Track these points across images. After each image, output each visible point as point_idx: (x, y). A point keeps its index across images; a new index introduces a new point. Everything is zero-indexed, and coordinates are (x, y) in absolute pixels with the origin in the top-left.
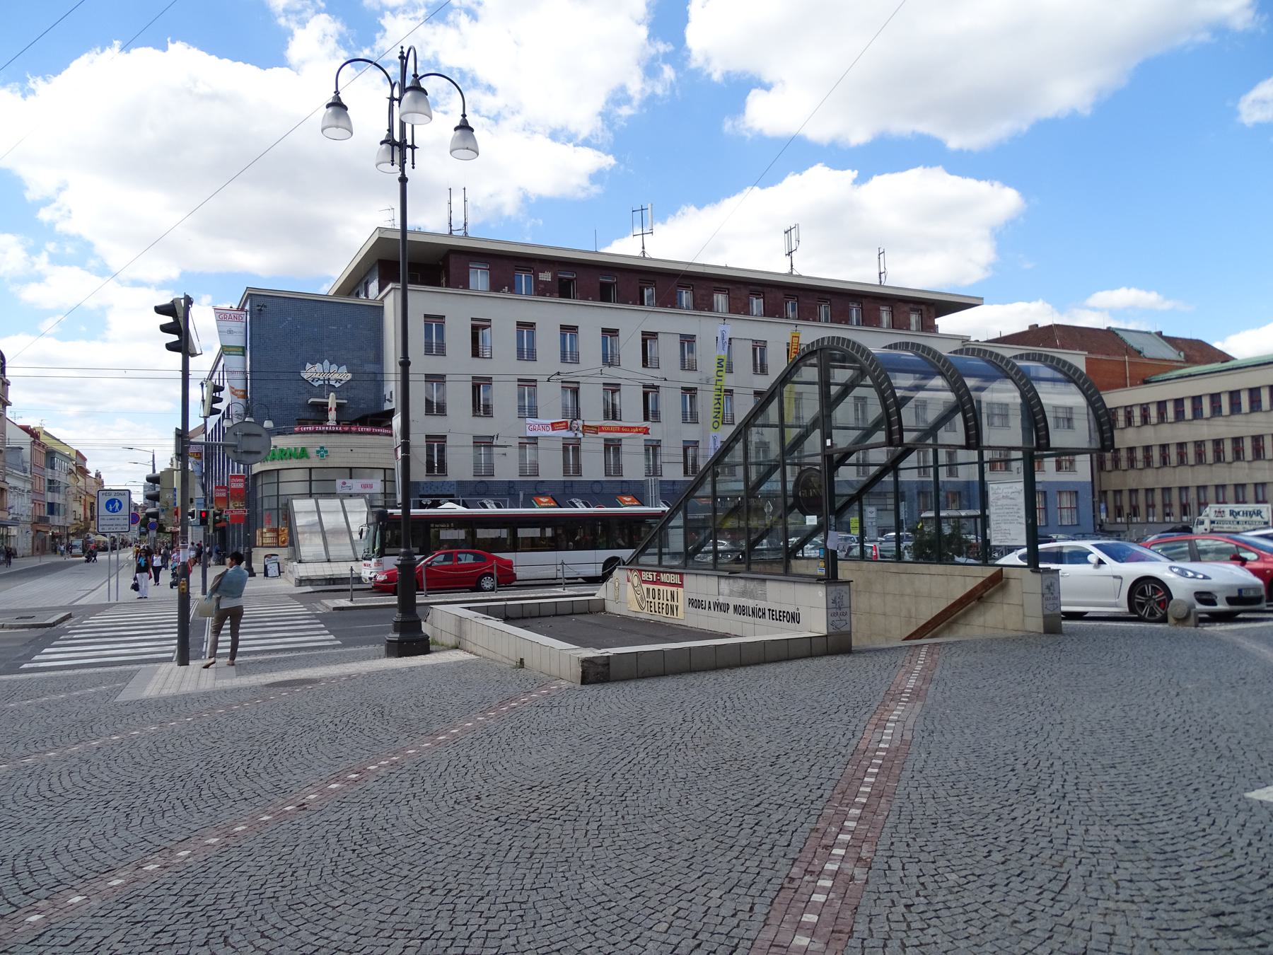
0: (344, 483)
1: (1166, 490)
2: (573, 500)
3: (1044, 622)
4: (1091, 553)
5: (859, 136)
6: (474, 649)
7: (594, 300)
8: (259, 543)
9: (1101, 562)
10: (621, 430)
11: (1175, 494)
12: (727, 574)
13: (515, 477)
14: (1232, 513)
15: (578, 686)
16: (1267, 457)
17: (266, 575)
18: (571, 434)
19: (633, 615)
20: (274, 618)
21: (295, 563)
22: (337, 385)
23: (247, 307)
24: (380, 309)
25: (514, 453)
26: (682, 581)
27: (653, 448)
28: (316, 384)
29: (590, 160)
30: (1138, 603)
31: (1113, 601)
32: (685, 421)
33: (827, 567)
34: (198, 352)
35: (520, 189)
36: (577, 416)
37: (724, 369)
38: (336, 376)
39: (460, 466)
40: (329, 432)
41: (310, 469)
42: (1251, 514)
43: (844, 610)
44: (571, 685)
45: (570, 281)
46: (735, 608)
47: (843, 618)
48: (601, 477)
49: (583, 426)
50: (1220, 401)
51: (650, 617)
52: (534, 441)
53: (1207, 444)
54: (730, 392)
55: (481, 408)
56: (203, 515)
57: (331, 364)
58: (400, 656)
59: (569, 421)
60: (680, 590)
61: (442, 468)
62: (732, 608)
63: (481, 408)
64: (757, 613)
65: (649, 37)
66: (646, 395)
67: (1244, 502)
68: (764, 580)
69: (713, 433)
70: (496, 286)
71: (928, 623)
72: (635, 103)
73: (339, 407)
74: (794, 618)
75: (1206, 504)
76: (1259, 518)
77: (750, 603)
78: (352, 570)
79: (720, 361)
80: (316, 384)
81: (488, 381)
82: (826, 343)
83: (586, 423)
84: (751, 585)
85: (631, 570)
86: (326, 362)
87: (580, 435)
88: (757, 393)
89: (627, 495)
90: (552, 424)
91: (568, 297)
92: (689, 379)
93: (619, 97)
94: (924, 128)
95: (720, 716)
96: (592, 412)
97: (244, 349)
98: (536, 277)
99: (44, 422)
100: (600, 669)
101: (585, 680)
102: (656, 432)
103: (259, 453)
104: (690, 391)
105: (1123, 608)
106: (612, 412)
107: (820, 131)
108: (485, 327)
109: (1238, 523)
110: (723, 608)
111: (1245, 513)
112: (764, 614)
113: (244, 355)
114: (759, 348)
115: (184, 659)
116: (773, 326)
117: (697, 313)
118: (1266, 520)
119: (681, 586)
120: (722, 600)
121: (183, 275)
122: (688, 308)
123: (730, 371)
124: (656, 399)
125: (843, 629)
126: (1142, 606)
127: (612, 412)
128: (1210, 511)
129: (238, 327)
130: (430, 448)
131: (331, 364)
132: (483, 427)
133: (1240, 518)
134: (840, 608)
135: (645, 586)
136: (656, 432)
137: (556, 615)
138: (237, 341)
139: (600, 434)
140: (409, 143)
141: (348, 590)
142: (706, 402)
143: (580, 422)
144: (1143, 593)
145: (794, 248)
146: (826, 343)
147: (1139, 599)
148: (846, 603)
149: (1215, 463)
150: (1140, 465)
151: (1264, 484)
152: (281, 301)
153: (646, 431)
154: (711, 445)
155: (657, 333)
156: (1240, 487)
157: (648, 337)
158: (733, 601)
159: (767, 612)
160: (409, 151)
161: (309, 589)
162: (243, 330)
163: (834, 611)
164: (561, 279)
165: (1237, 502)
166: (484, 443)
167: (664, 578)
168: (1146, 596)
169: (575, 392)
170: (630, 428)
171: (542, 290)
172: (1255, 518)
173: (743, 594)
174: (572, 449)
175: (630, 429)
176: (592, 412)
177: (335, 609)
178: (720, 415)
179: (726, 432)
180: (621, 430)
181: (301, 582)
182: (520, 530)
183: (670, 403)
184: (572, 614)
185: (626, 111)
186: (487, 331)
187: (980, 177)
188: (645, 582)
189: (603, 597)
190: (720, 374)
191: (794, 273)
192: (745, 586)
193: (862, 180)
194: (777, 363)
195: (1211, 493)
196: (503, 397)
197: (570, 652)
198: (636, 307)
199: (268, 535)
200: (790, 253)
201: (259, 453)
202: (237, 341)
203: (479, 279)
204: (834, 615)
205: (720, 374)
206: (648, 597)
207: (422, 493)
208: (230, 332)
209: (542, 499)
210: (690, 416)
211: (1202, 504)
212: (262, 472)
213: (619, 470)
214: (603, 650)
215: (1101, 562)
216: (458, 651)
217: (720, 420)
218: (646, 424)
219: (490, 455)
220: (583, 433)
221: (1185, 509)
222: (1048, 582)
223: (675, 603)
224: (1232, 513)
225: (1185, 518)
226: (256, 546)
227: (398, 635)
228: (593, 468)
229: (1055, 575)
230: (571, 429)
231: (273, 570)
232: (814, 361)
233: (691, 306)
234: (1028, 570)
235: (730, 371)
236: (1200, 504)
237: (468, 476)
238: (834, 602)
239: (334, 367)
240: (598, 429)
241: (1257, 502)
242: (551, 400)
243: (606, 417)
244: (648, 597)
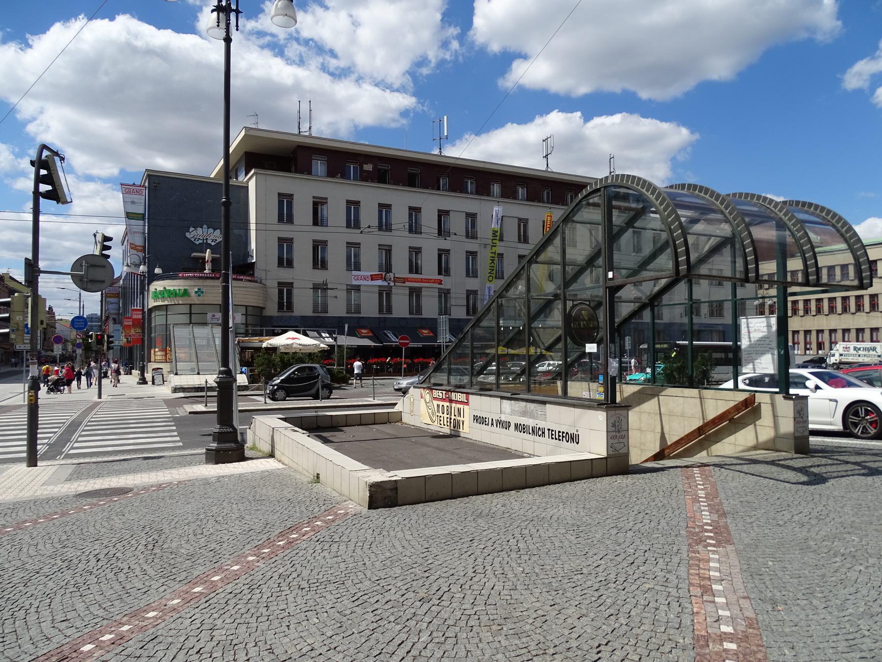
0: (214, 316)
1: (807, 332)
2: (385, 332)
3: (795, 444)
4: (808, 379)
5: (583, 90)
6: (283, 459)
8: (152, 360)
9: (817, 387)
10: (422, 281)
11: (814, 334)
12: (509, 395)
13: (343, 314)
14: (855, 348)
15: (365, 510)
16: (865, 311)
17: (153, 383)
18: (385, 284)
19: (426, 426)
20: (139, 421)
21: (172, 375)
22: (213, 244)
23: (147, 184)
24: (246, 188)
25: (343, 295)
26: (467, 399)
27: (444, 295)
28: (197, 243)
29: (405, 101)
30: (852, 423)
31: (829, 419)
32: (468, 275)
33: (606, 392)
34: (69, 200)
35: (353, 120)
36: (389, 269)
38: (212, 237)
39: (303, 305)
40: (207, 278)
41: (191, 305)
42: (868, 349)
43: (623, 433)
44: (359, 508)
45: (386, 171)
46: (516, 426)
47: (621, 440)
48: (406, 315)
50: (848, 269)
51: (439, 429)
52: (357, 288)
53: (851, 298)
54: (501, 256)
55: (319, 263)
56: (99, 337)
57: (208, 228)
58: (217, 463)
59: (384, 274)
60: (466, 406)
61: (290, 307)
62: (513, 426)
63: (319, 263)
64: (537, 432)
65: (442, 20)
66: (440, 256)
67: (863, 341)
68: (544, 403)
69: (488, 284)
70: (331, 173)
71: (682, 439)
72: (433, 65)
73: (214, 261)
74: (573, 438)
75: (836, 343)
76: (874, 353)
77: (530, 422)
78: (206, 382)
79: (495, 232)
80: (197, 243)
81: (324, 243)
82: (609, 181)
84: (532, 406)
85: (424, 388)
87: (392, 284)
88: (521, 257)
89: (425, 329)
90: (371, 275)
91: (385, 182)
92: (472, 246)
93: (422, 62)
94: (631, 87)
95: (514, 564)
96: (400, 267)
97: (144, 215)
98: (362, 168)
99: (10, 270)
100: (389, 493)
101: (373, 504)
102: (447, 282)
103: (103, 282)
104: (472, 254)
105: (839, 427)
106: (415, 268)
107: (558, 86)
108: (323, 204)
109: (859, 356)
110: (506, 425)
111: (865, 349)
112: (543, 433)
113: (144, 219)
114: (523, 223)
115: (32, 460)
116: (532, 208)
117: (478, 197)
118: (879, 354)
119: (467, 403)
120: (503, 418)
121: (122, 172)
122: (471, 193)
123: (501, 240)
125: (621, 451)
126: (856, 425)
127: (415, 268)
128: (840, 347)
130: (281, 292)
131: (208, 228)
132: (319, 276)
133: (860, 352)
134: (619, 432)
135: (436, 403)
136: (447, 282)
137: (361, 425)
138: (140, 209)
139: (408, 284)
140: (233, 7)
141: (203, 397)
142: (483, 264)
143: (392, 275)
144: (856, 414)
145: (549, 152)
146: (609, 181)
147: (853, 419)
148: (624, 427)
149: (871, 311)
150: (801, 313)
151: (877, 329)
153: (440, 282)
154: (487, 292)
155: (449, 211)
156: (860, 331)
157: (442, 214)
158: (514, 420)
159: (546, 432)
160: (233, 16)
161: (182, 395)
162: (143, 201)
163: (614, 434)
164: (379, 170)
165: (858, 341)
166: (320, 288)
167: (453, 396)
168: (859, 417)
171: (365, 177)
172: (871, 352)
173: (524, 414)
174: (385, 295)
175: (428, 281)
176: (400, 267)
177: (190, 413)
178: (494, 272)
179: (497, 285)
180: (422, 281)
181: (176, 390)
182: (723, 357)
183: (457, 263)
184: (374, 424)
185: (425, 71)
186: (325, 207)
187: (662, 120)
188: (435, 399)
189: (401, 410)
190: (494, 241)
191: (549, 170)
192: (526, 407)
193: (587, 118)
194: (536, 236)
195: (839, 334)
196: (336, 255)
197: (360, 474)
198: (434, 192)
199: (159, 353)
200: (546, 156)
201: (103, 282)
202: (140, 209)
203: (319, 166)
204: (613, 438)
205: (494, 241)
206: (438, 411)
207: (274, 324)
208: (133, 202)
209: (363, 331)
210: (471, 272)
211: (833, 343)
212: (155, 307)
213: (419, 310)
214: (392, 473)
215: (817, 387)
216: (271, 460)
217: (494, 276)
219: (325, 297)
220: (395, 281)
221: (820, 346)
222: (799, 408)
223: (461, 419)
224: (855, 348)
225: (820, 352)
226: (150, 362)
227: (216, 445)
228: (401, 308)
229: (804, 401)
230: (385, 280)
231: (158, 379)
232: (595, 199)
233: (474, 191)
234: (781, 396)
235: (501, 240)
236: (831, 343)
237: (308, 312)
238: (614, 425)
239: (211, 230)
240: (405, 280)
241: (872, 341)
242: (370, 259)
243: (411, 271)
244: (438, 411)
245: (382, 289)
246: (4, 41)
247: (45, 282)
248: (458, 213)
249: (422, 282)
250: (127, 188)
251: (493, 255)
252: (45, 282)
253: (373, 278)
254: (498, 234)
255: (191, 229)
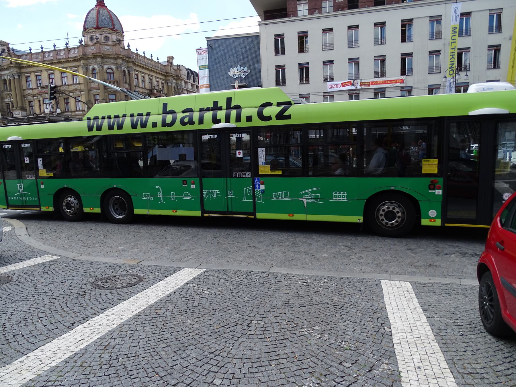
7: (369, 6)
10: (385, 82)
28: (235, 77)
36: (357, 77)
37: (457, 34)
49: (361, 83)
59: (352, 81)
83: (362, 81)
86: (239, 66)
90: (342, 83)
124: (410, 63)
129: (205, 56)
139: (372, 87)
152: (233, 39)
155: (471, 12)
169: (383, 61)
170: (391, 81)
175: (391, 82)
180: (385, 82)
190: (453, 38)
205: (453, 38)
218: (404, 77)
230: (353, 85)
245: (351, 92)
246: (97, 1)
247: (512, 144)
248: (421, 19)
249: (385, 83)
250: (199, 51)
251: (453, 51)
252: (512, 144)
253: (343, 85)
254: (457, 30)
255: (231, 69)
